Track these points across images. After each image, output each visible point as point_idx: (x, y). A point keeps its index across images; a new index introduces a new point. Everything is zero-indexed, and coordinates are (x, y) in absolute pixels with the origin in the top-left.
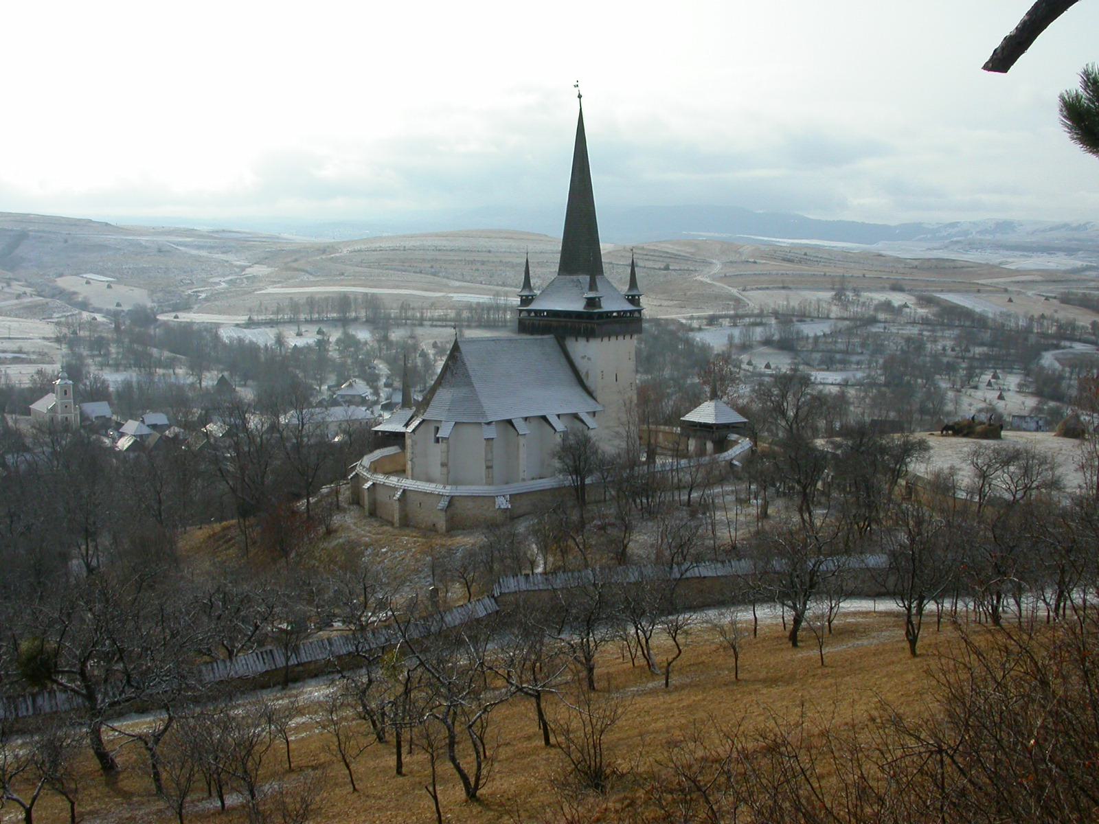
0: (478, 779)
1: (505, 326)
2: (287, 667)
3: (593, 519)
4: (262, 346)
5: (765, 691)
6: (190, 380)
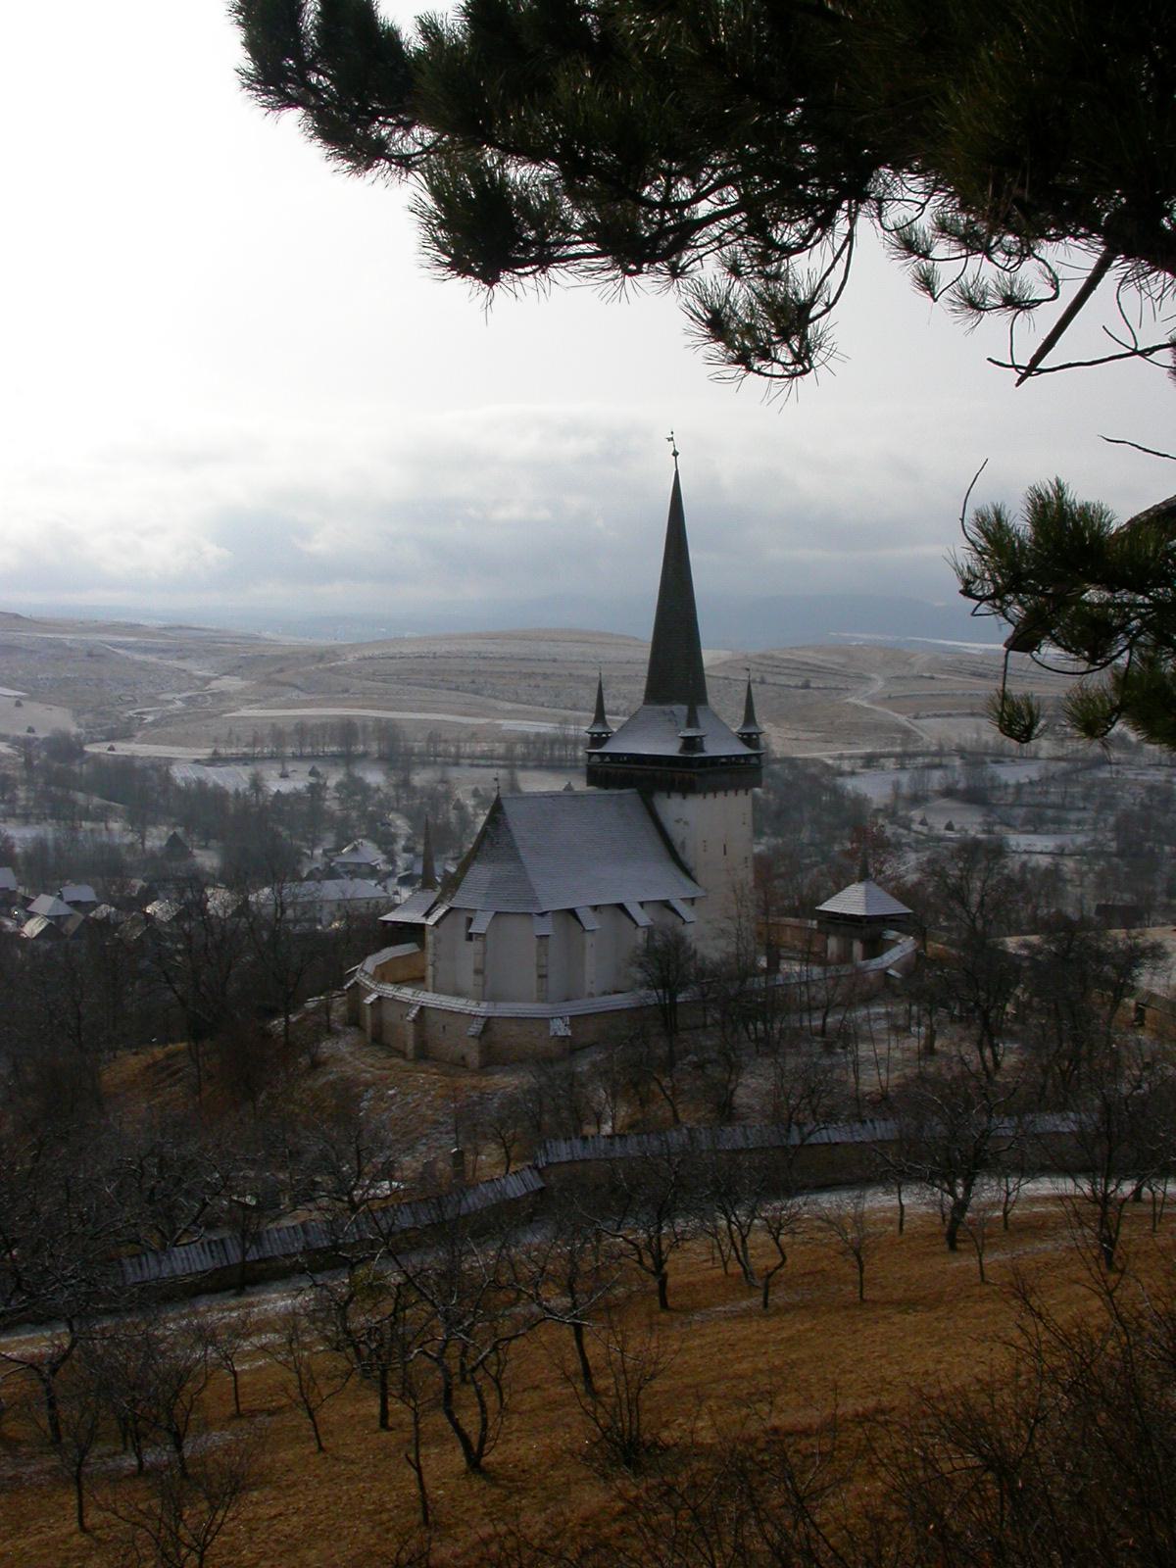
0: (483, 1441)
1: (576, 767)
2: (244, 1264)
3: (687, 1052)
4: (231, 791)
5: (897, 1318)
6: (129, 838)
